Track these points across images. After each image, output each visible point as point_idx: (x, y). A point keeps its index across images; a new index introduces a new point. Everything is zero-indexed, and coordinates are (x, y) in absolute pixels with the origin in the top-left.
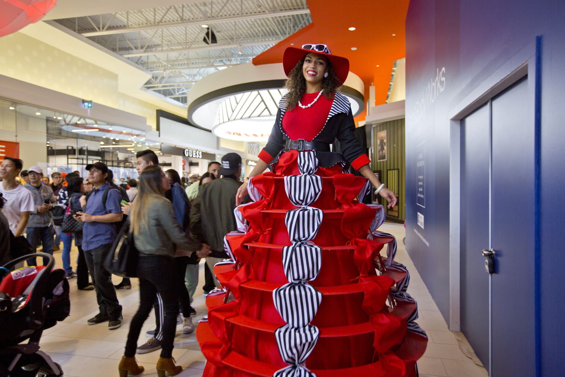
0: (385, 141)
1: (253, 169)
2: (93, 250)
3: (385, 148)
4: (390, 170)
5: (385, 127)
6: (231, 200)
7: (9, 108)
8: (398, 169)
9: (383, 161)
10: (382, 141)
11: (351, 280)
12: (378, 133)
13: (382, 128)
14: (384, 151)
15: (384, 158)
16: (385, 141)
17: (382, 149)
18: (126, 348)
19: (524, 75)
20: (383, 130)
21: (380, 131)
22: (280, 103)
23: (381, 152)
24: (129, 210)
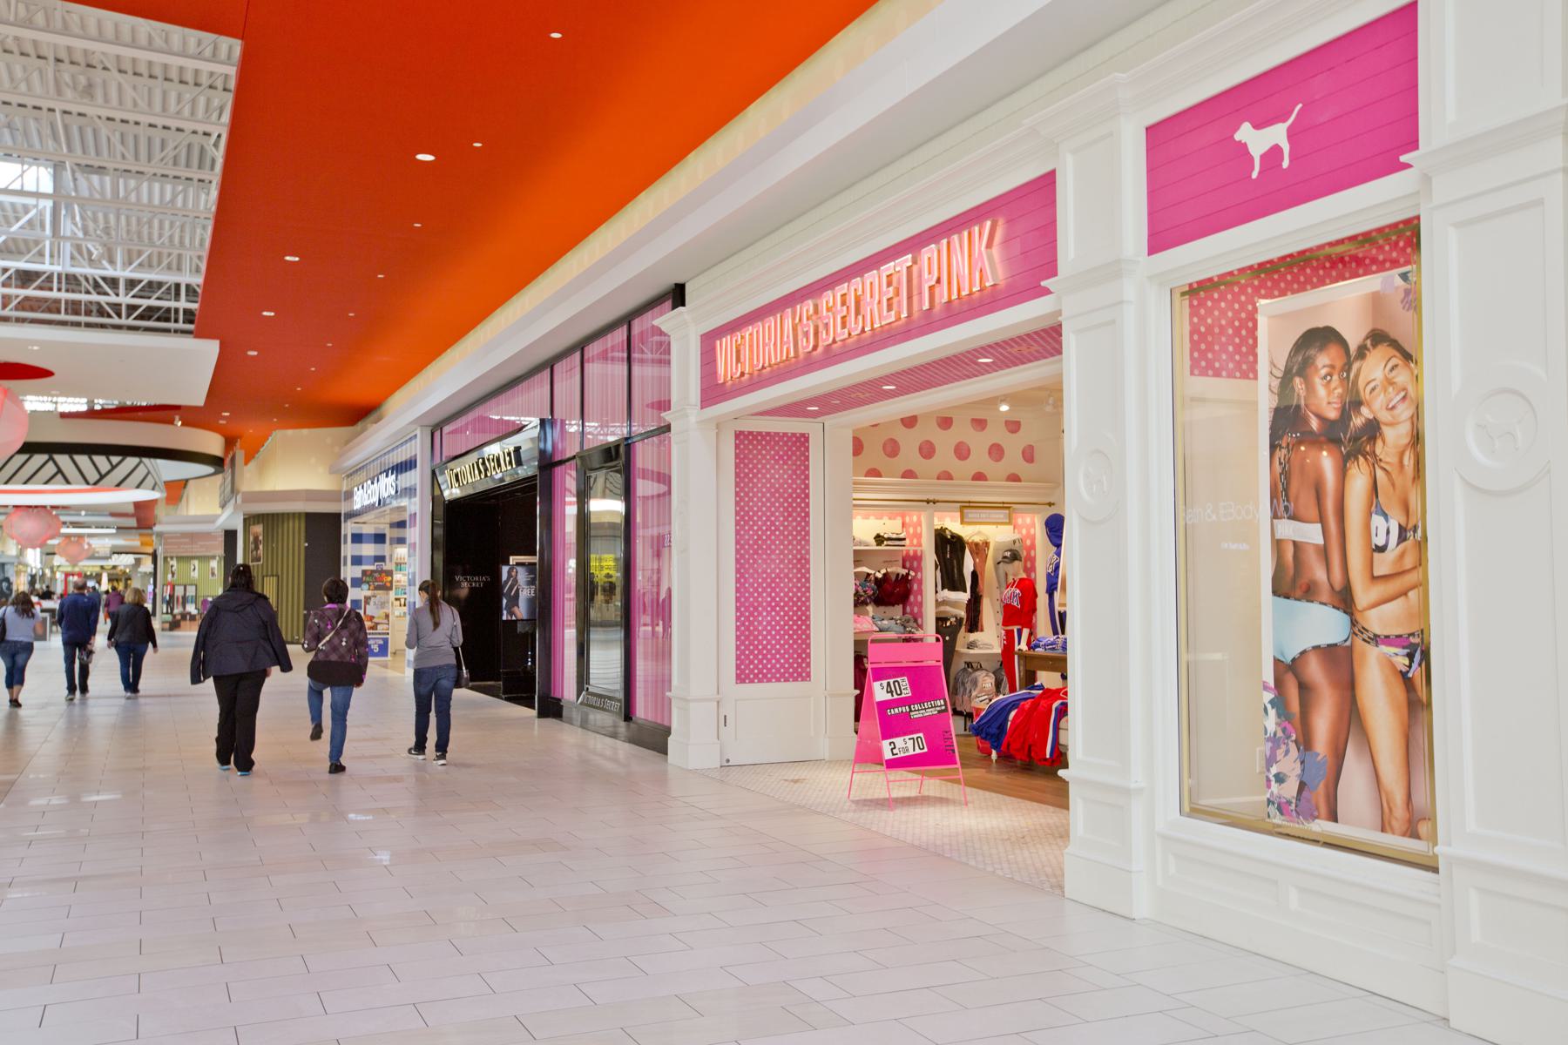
0: (261, 538)
1: (442, 558)
2: (1025, 666)
3: (261, 547)
4: (267, 576)
5: (261, 520)
6: (1049, 575)
7: (227, 423)
8: (277, 576)
9: (258, 565)
10: (256, 539)
11: (470, 684)
12: (251, 527)
13: (256, 521)
14: (259, 552)
15: (259, 560)
16: (261, 538)
17: (257, 548)
18: (218, 740)
19: (70, 480)
20: (258, 523)
21: (254, 524)
22: (1048, 340)
23: (255, 552)
24: (260, 623)
